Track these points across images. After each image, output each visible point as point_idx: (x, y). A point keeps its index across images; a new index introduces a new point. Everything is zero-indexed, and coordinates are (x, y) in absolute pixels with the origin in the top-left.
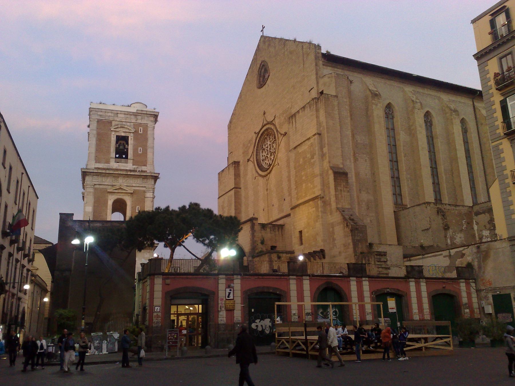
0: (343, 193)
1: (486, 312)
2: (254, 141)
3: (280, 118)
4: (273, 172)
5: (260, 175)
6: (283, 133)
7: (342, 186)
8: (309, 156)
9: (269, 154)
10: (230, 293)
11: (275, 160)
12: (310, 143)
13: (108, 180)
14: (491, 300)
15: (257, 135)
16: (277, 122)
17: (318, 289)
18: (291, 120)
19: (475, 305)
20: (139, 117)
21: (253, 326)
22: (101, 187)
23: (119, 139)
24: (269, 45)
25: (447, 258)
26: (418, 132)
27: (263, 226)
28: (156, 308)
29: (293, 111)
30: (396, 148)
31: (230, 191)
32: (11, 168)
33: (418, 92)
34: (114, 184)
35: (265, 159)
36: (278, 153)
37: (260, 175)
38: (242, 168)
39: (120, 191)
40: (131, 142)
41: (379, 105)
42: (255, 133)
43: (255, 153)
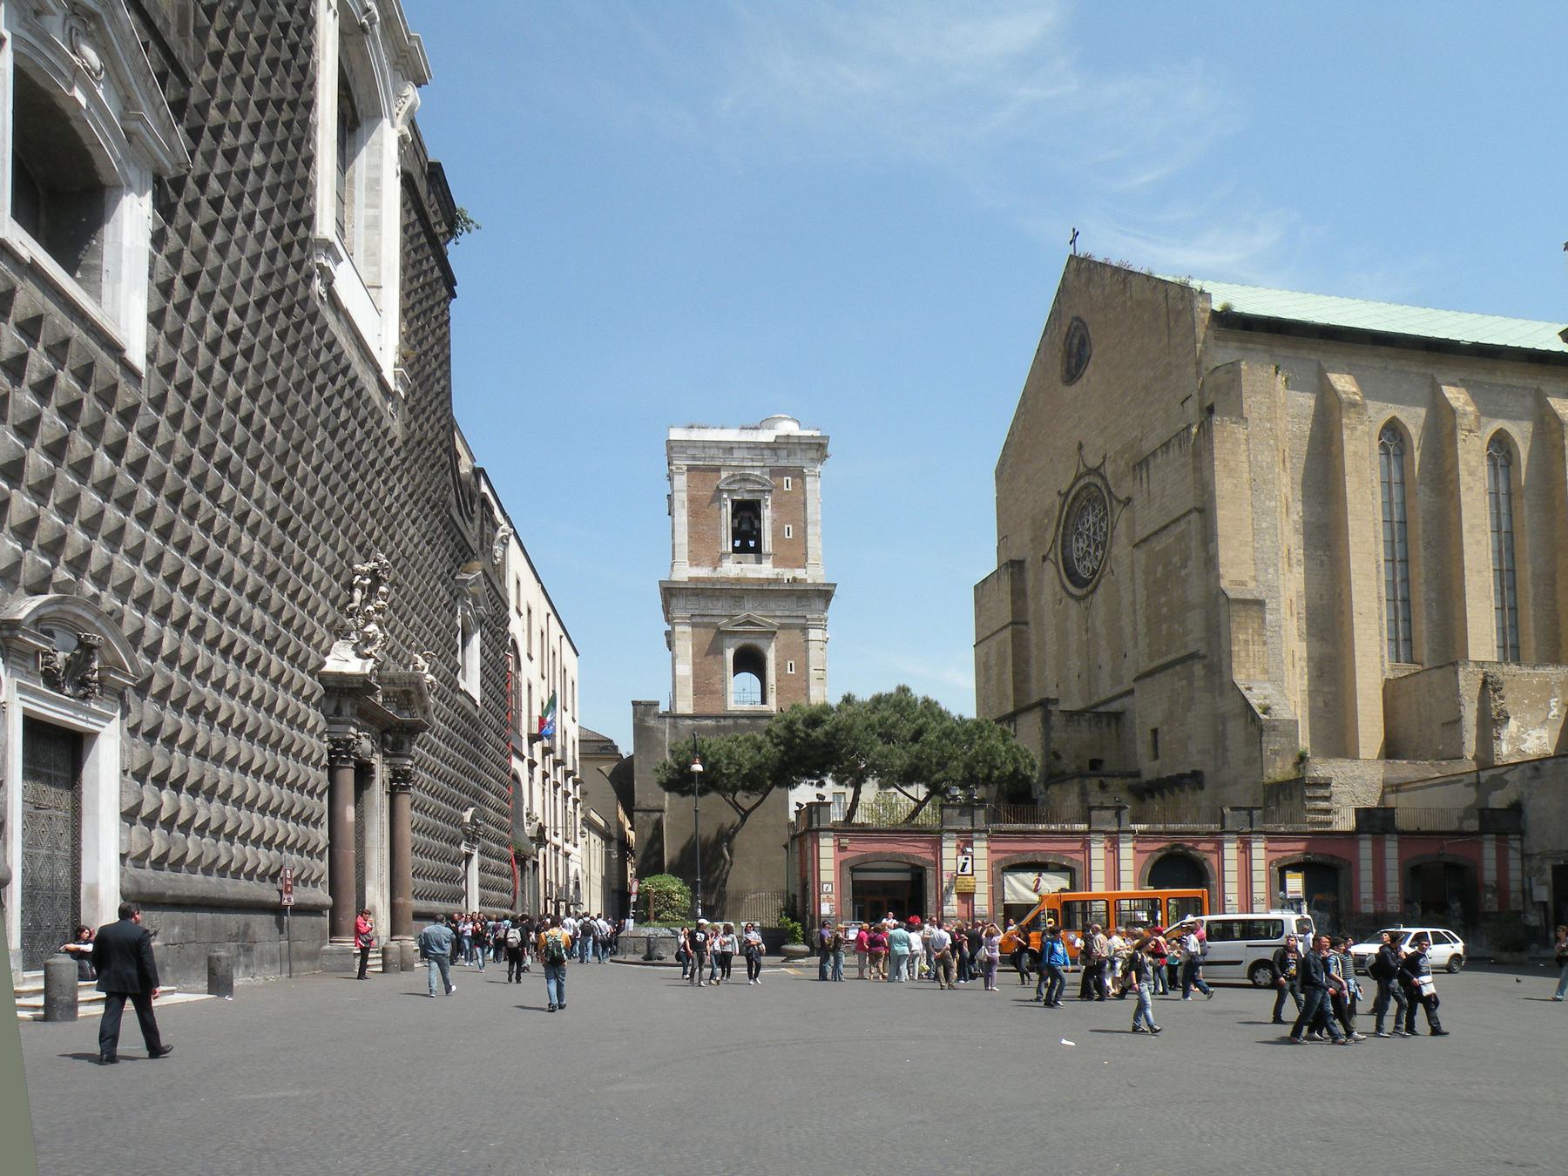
1: (1535, 899)
2: (1057, 513)
3: (1115, 461)
4: (1100, 590)
5: (1071, 595)
6: (1123, 498)
8: (1176, 560)
9: (1093, 547)
10: (965, 865)
11: (1105, 563)
12: (1179, 530)
13: (720, 603)
14: (1548, 876)
15: (1063, 498)
16: (1109, 470)
18: (1137, 471)
19: (1514, 886)
20: (784, 453)
24: (1089, 280)
25: (1472, 789)
26: (1462, 489)
27: (1071, 715)
28: (825, 886)
29: (1147, 447)
30: (1406, 527)
31: (1001, 629)
32: (529, 611)
33: (1476, 382)
34: (733, 612)
35: (1084, 558)
36: (1111, 547)
37: (1071, 595)
38: (1030, 575)
39: (748, 628)
40: (767, 514)
41: (1360, 427)
42: (1059, 493)
43: (1060, 542)
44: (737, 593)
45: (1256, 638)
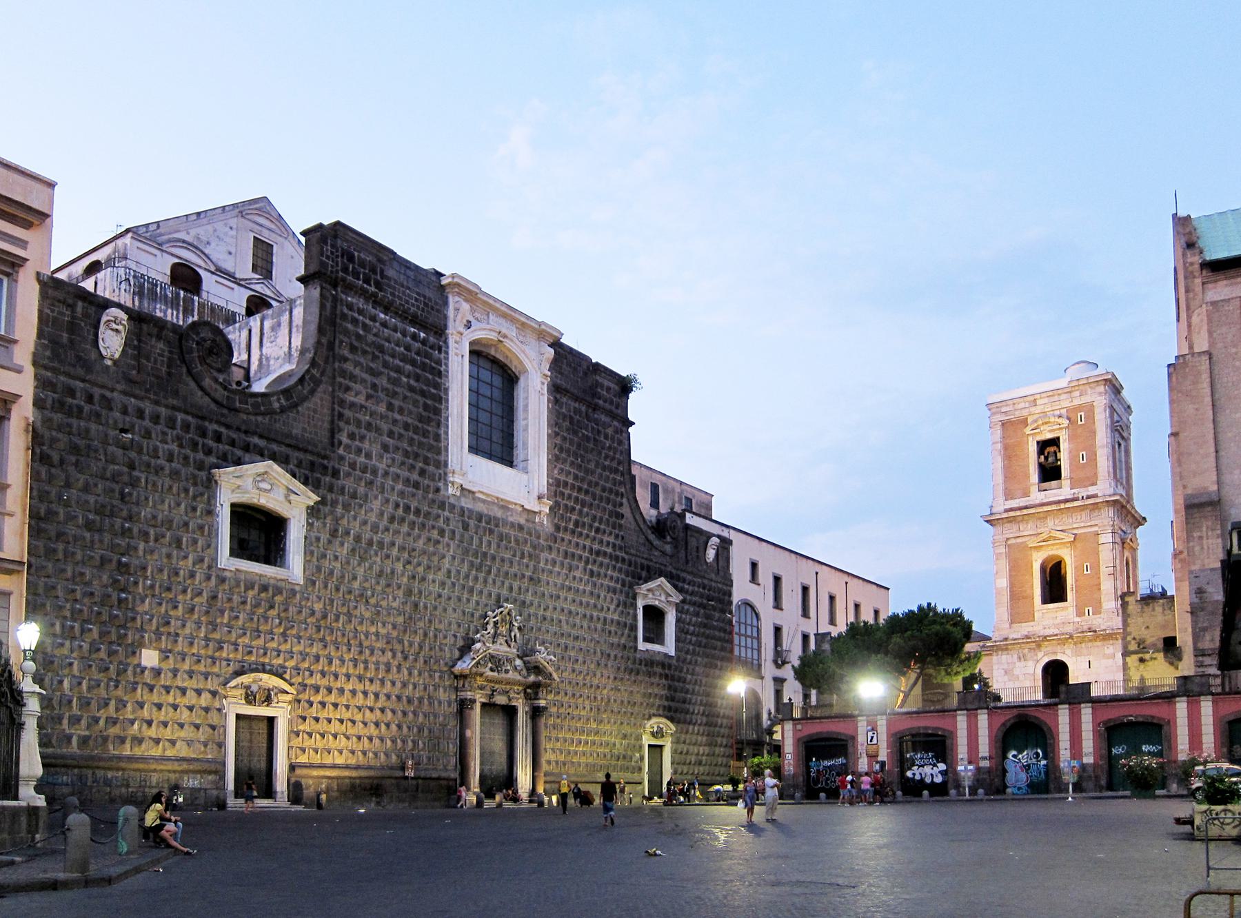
0: (1205, 542)
7: (1204, 529)
10: (872, 737)
17: (1004, 724)
20: (1077, 394)
21: (909, 774)
22: (1019, 540)
23: (1043, 446)
32: (777, 580)
34: (1039, 531)
40: (1064, 445)
44: (1042, 515)
45: (1210, 533)
